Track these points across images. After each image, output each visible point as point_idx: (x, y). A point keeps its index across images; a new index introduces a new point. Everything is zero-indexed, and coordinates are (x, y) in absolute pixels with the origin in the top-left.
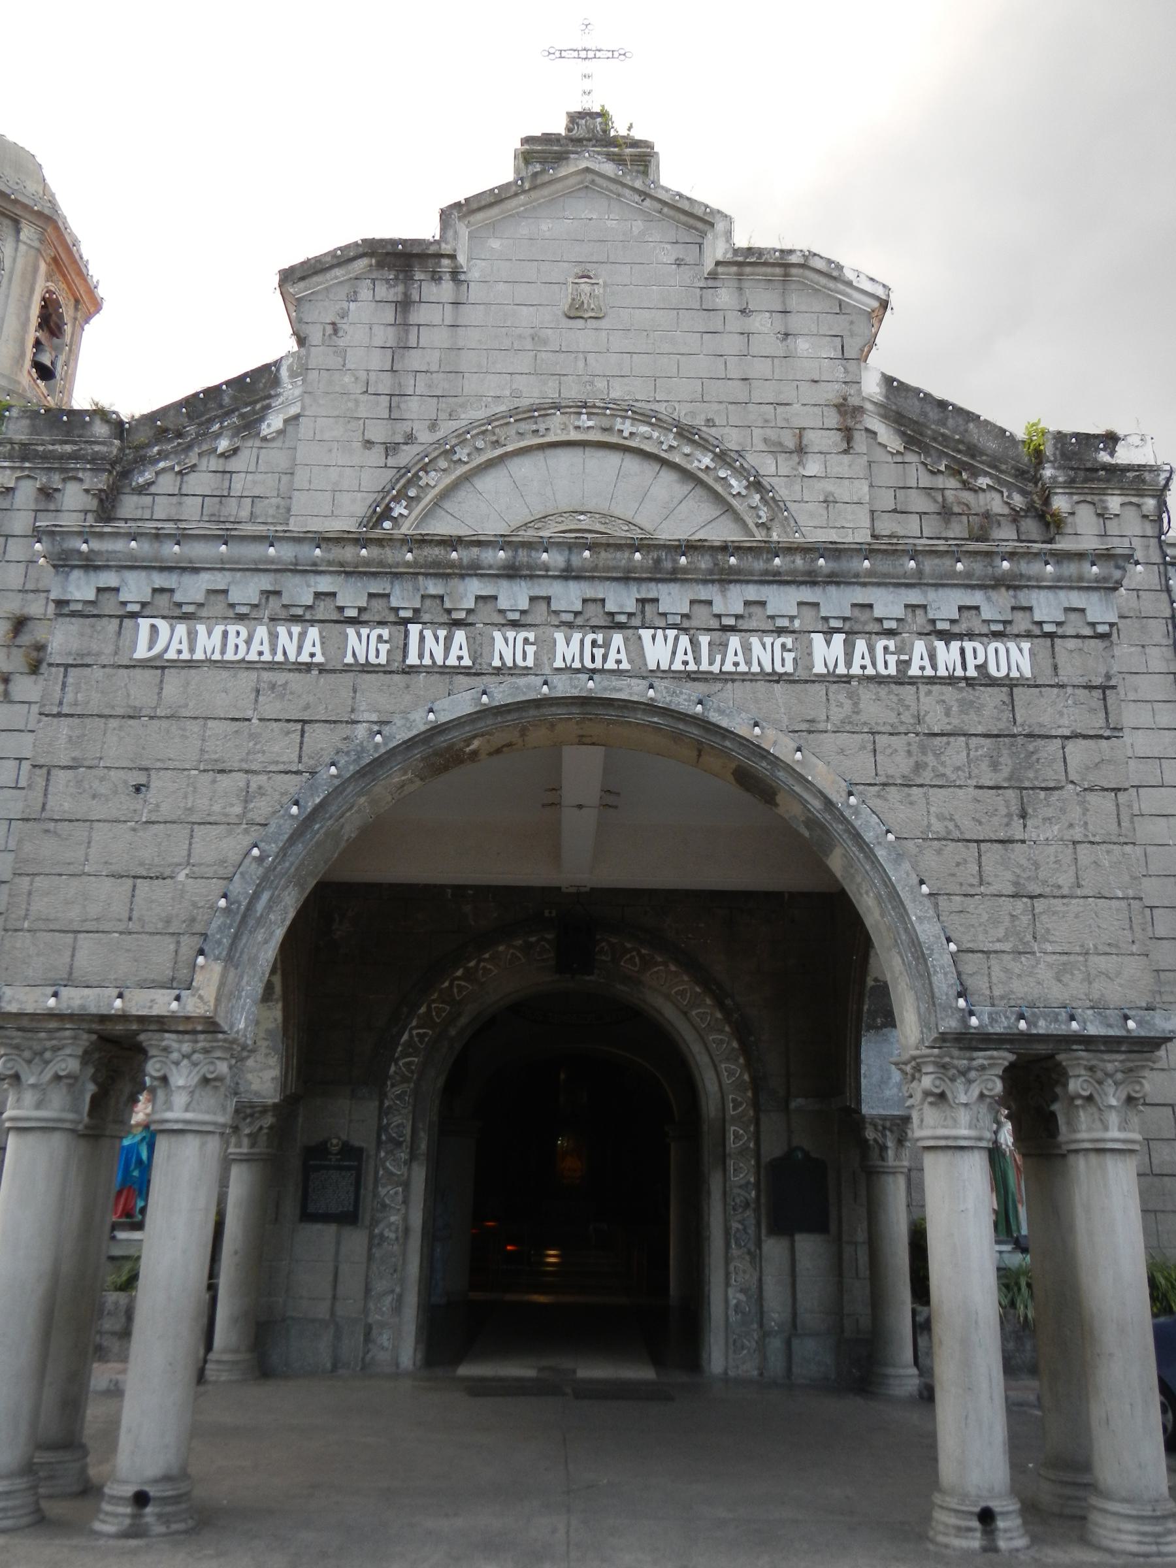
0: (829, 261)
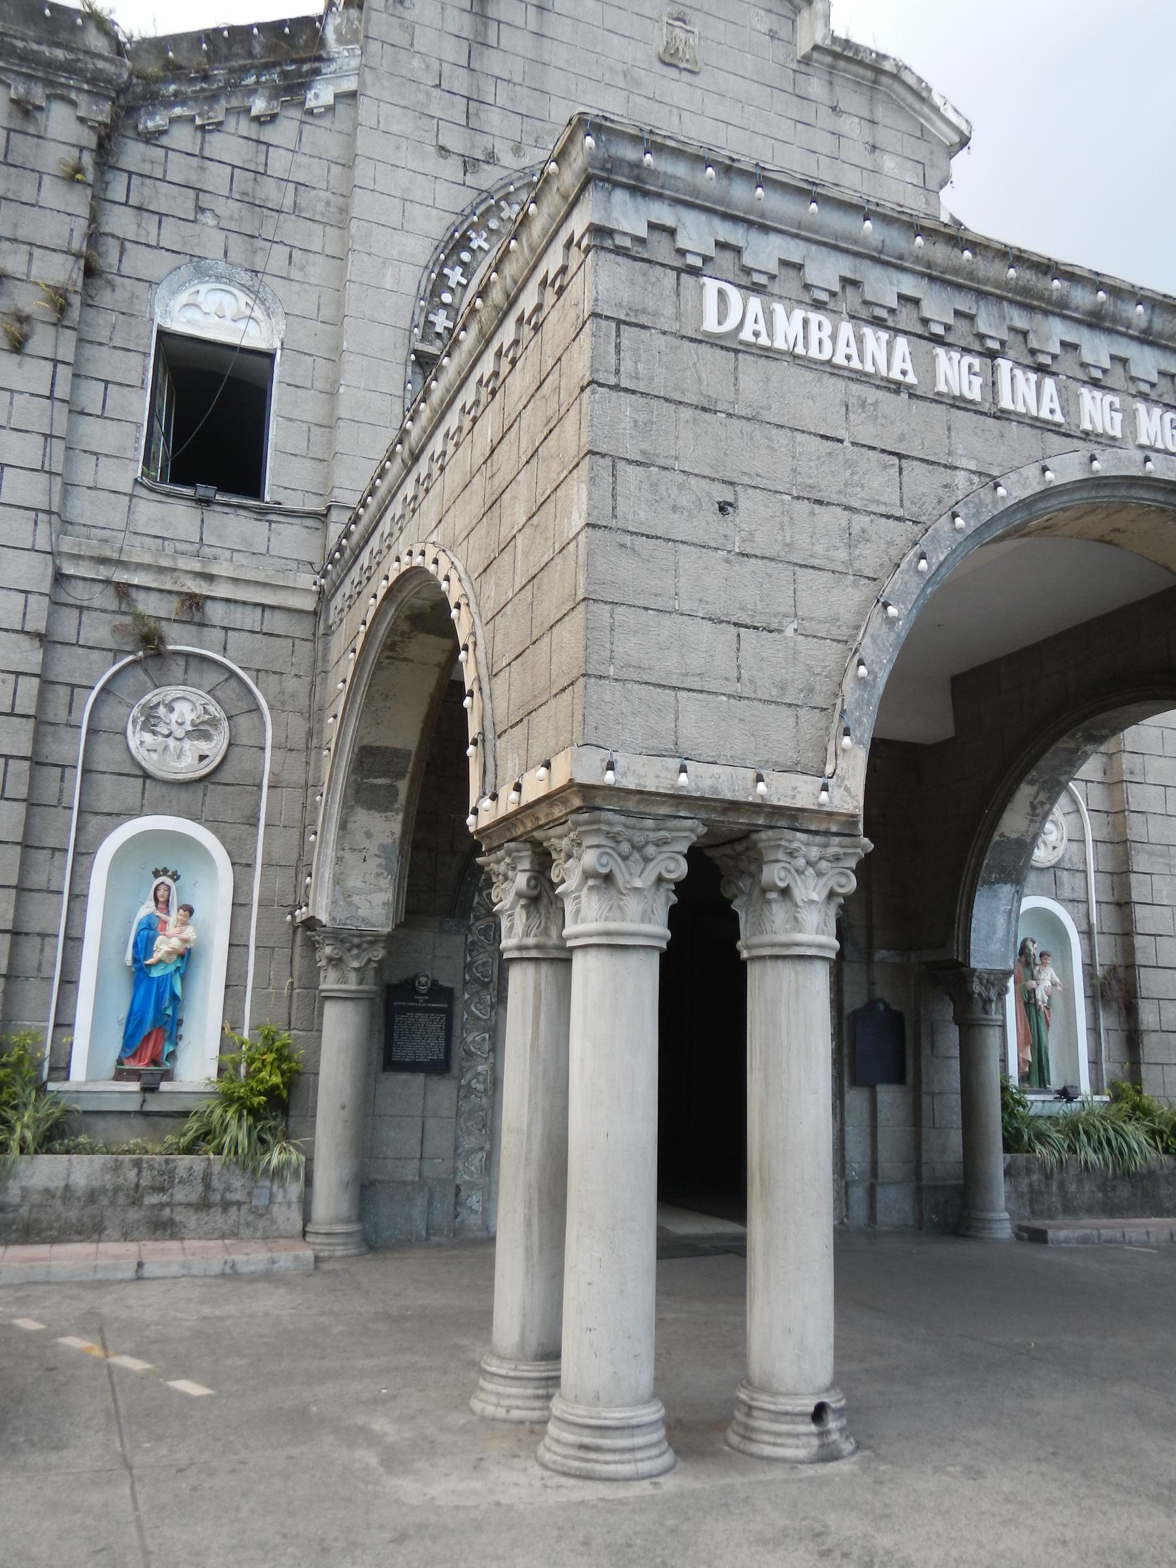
0: (920, 80)
